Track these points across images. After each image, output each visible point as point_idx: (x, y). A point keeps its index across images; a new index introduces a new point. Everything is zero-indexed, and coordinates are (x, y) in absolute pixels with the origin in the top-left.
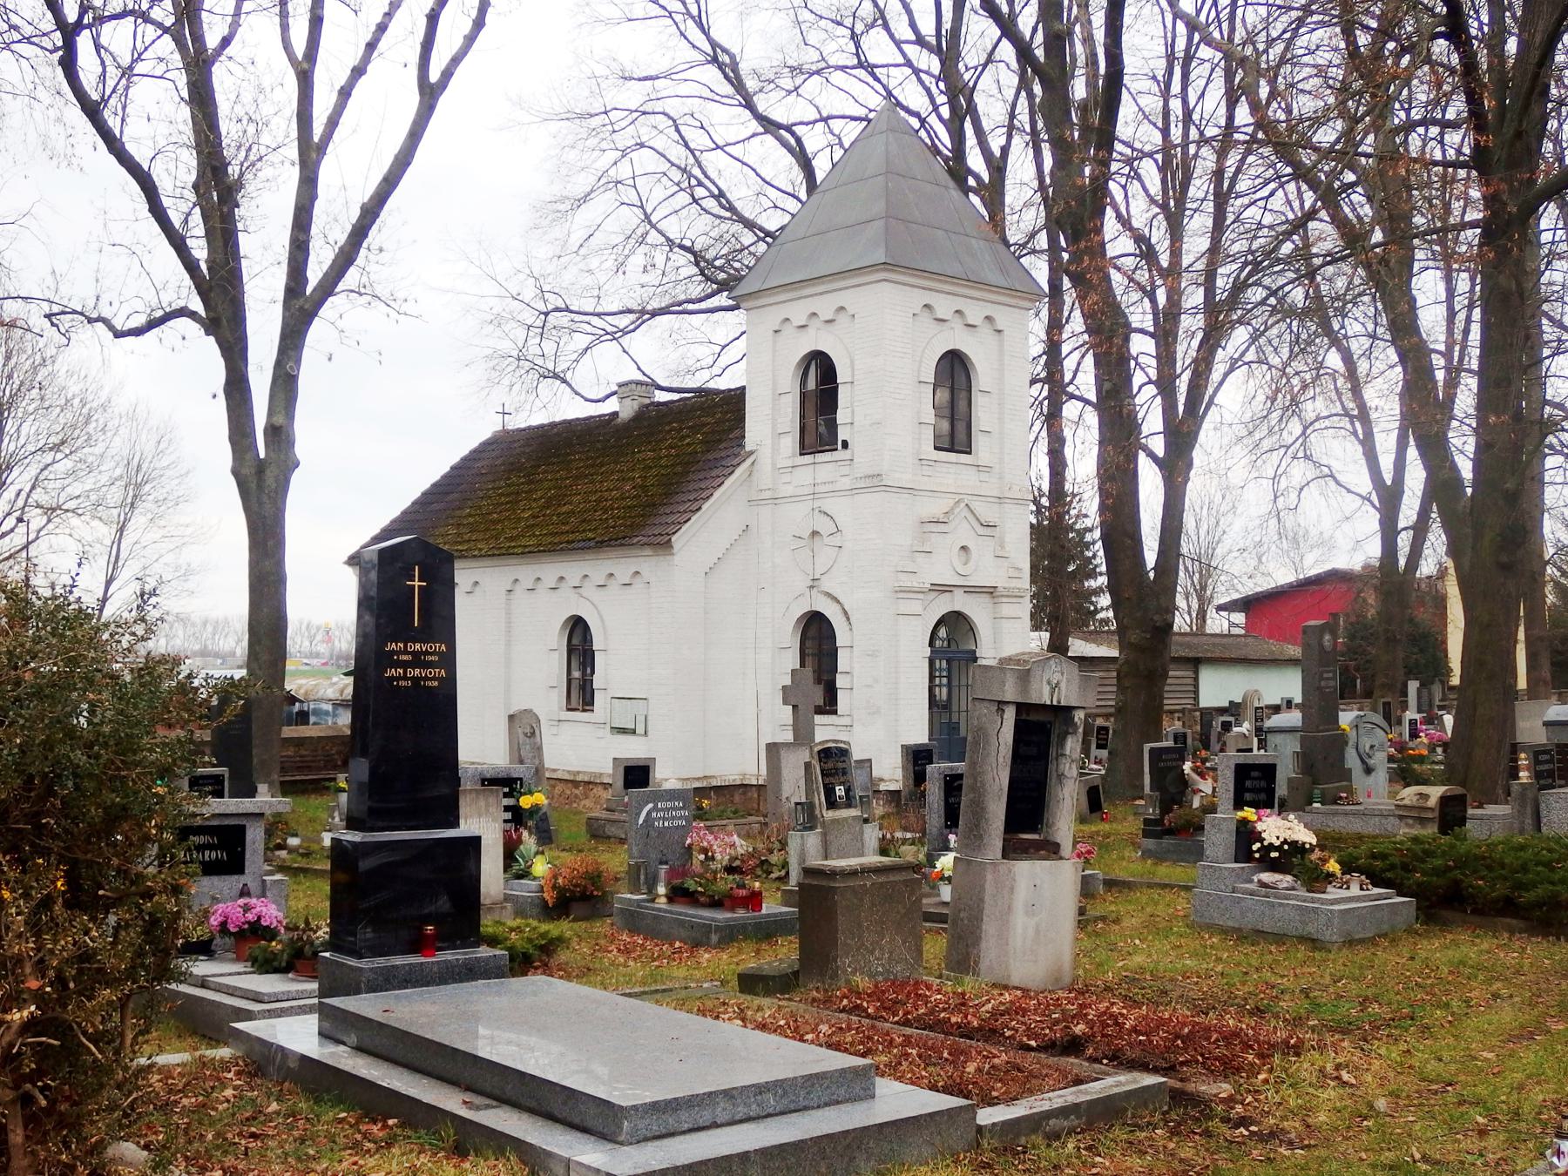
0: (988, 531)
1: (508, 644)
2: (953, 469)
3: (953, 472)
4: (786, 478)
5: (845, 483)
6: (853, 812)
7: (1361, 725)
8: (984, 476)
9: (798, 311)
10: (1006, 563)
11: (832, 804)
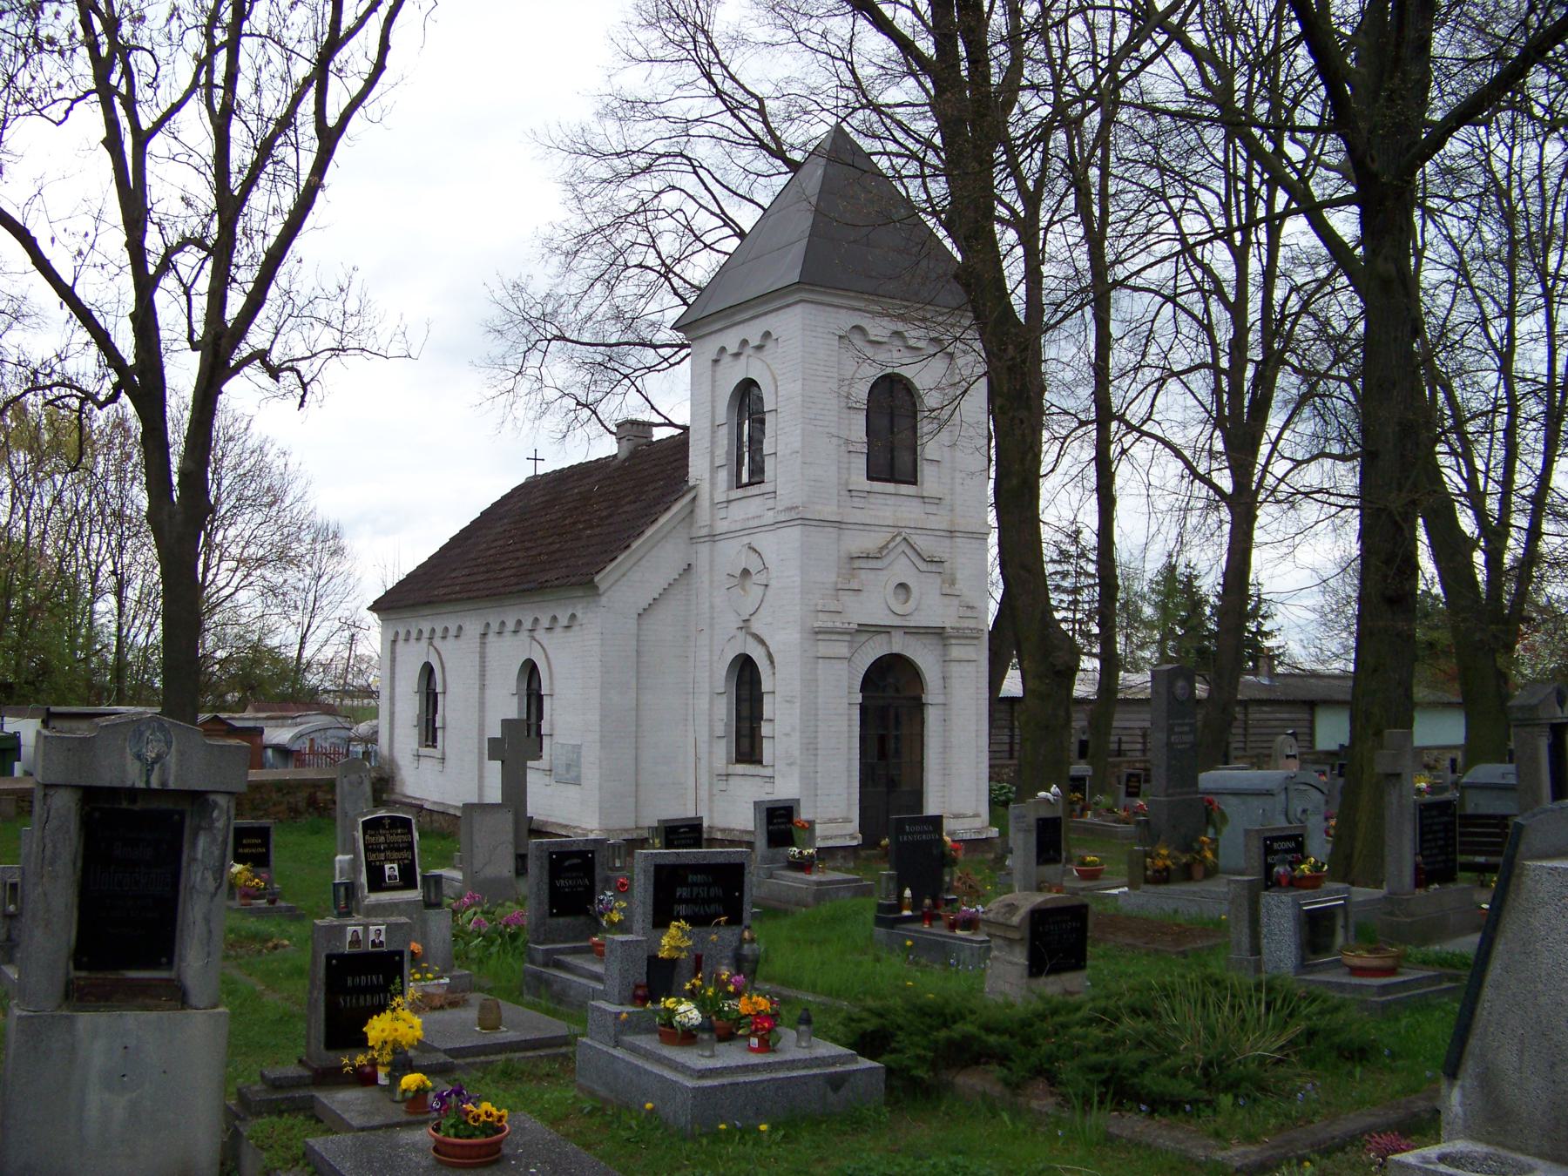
0: (933, 568)
1: (483, 687)
2: (891, 500)
3: (893, 506)
4: (722, 514)
5: (770, 517)
6: (415, 895)
7: (1292, 787)
8: (931, 509)
9: (731, 340)
10: (956, 602)
11: (377, 882)
